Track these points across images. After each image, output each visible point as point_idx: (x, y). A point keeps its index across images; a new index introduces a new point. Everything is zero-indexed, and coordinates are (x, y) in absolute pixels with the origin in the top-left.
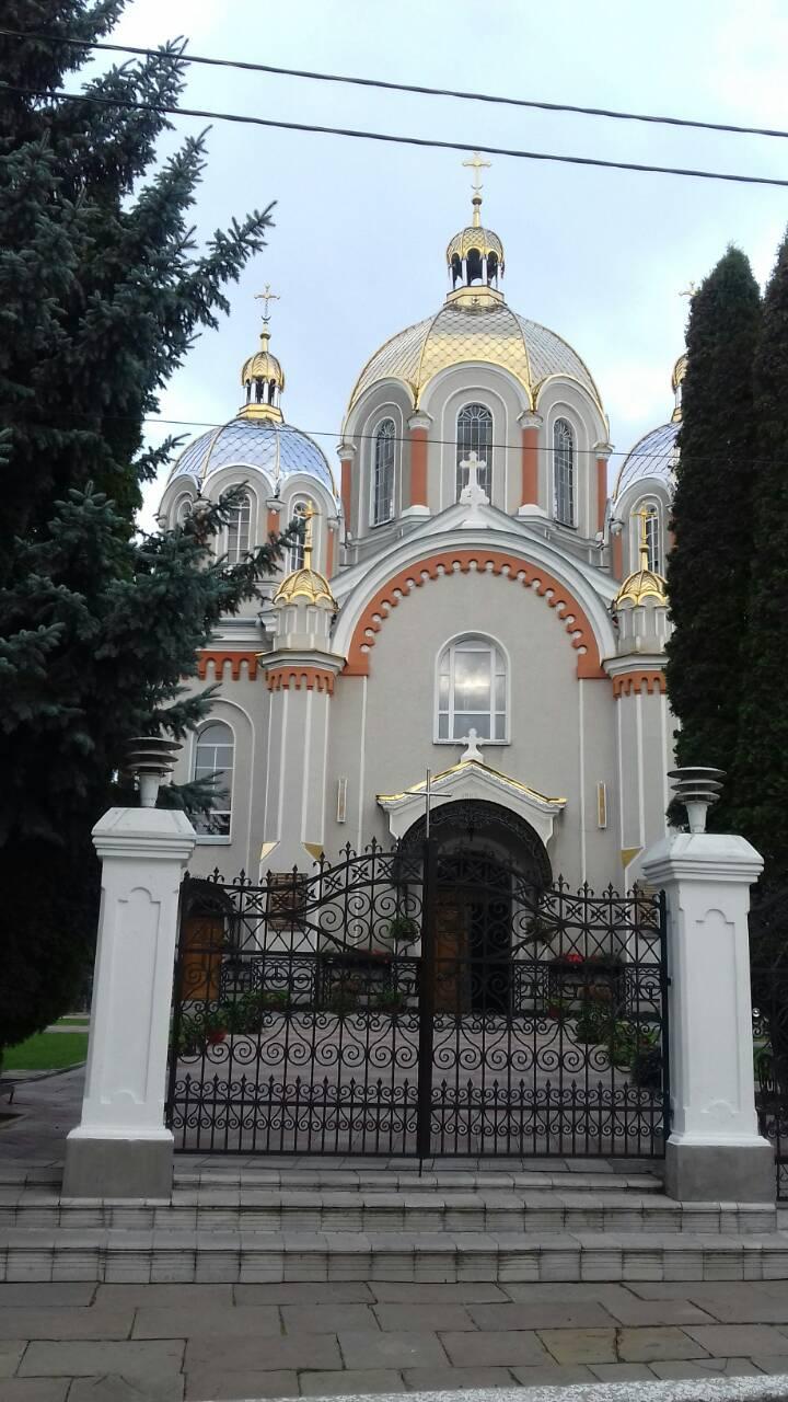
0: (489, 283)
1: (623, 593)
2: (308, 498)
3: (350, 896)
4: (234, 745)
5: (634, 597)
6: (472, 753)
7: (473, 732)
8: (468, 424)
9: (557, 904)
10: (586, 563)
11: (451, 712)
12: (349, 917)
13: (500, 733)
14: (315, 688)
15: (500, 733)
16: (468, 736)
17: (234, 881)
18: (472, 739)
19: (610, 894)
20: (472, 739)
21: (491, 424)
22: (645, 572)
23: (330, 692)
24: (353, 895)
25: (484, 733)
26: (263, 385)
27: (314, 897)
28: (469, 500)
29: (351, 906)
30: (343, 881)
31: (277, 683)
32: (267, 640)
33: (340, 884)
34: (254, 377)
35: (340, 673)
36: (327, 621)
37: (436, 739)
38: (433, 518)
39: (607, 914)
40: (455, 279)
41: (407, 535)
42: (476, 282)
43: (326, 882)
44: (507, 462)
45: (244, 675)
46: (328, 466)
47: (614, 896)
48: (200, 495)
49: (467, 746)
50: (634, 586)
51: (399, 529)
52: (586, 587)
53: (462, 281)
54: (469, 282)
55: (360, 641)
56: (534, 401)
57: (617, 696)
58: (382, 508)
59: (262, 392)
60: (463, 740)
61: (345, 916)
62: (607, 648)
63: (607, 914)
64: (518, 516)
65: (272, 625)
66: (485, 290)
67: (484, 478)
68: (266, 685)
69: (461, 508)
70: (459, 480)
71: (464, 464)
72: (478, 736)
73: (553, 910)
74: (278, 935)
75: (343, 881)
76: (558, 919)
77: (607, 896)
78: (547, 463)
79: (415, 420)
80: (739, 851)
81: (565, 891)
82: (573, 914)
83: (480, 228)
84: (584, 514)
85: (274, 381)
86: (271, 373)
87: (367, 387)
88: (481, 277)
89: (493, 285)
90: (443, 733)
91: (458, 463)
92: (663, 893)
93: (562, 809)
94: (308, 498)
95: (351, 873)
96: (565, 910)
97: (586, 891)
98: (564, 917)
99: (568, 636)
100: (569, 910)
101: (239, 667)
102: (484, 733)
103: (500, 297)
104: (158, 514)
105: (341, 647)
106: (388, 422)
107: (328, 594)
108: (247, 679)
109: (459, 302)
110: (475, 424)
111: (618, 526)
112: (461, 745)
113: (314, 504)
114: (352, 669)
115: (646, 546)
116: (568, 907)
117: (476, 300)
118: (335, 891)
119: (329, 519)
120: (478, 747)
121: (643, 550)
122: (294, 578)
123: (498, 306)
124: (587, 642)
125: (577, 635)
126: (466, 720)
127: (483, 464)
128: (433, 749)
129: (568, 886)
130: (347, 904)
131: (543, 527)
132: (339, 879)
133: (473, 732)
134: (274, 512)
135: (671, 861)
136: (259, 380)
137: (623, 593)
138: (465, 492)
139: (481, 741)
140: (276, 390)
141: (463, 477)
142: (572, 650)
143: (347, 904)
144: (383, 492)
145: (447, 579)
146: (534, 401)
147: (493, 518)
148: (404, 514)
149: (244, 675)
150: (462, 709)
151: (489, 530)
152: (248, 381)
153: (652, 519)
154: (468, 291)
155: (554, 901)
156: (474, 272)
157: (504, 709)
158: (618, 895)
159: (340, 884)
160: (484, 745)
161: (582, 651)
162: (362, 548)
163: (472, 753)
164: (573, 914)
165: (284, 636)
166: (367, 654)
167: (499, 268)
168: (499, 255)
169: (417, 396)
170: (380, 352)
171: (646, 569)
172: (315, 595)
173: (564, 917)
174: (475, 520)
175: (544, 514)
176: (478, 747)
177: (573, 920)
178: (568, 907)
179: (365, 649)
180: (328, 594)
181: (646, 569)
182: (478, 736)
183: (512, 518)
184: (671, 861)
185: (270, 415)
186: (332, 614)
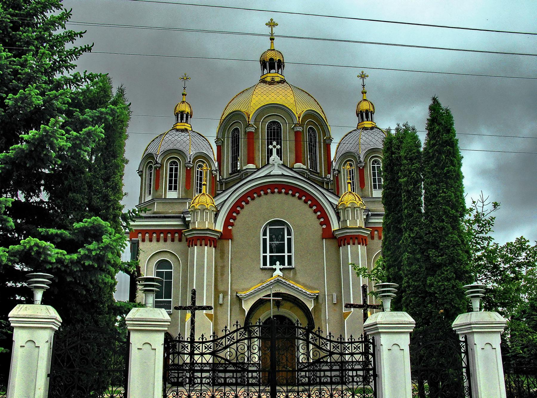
0: (278, 71)
1: (341, 202)
2: (204, 163)
3: (238, 344)
4: (173, 270)
5: (346, 204)
6: (278, 272)
7: (278, 263)
8: (271, 129)
9: (318, 340)
10: (323, 188)
11: (286, 254)
12: (238, 354)
13: (290, 263)
14: (208, 245)
15: (290, 263)
16: (276, 265)
17: (199, 339)
18: (278, 266)
19: (351, 339)
20: (278, 266)
21: (281, 129)
22: (350, 192)
23: (215, 247)
24: (240, 344)
25: (282, 263)
26: (183, 115)
27: (222, 345)
28: (274, 162)
29: (239, 348)
30: (235, 338)
31: (192, 242)
32: (186, 224)
33: (234, 339)
34: (179, 111)
35: (219, 239)
36: (213, 216)
37: (262, 266)
38: (258, 169)
39: (350, 348)
40: (264, 70)
41: (245, 178)
42: (272, 71)
43: (228, 338)
44: (288, 144)
45: (154, 239)
46: (211, 148)
47: (353, 340)
48: (157, 162)
49: (275, 269)
50: (346, 198)
51: (242, 174)
52: (325, 199)
53: (265, 71)
54: (270, 71)
55: (227, 223)
56: (299, 120)
57: (340, 246)
58: (234, 165)
59: (183, 118)
60: (274, 267)
61: (236, 353)
62: (335, 226)
63: (350, 348)
64: (293, 168)
65: (189, 217)
66: (276, 74)
67: (279, 152)
68: (186, 243)
69: (270, 165)
70: (268, 153)
71: (270, 147)
72: (280, 265)
73: (338, 350)
74: (208, 362)
75: (235, 338)
76: (330, 351)
77: (350, 341)
78: (306, 146)
79: (248, 128)
80: (405, 317)
81: (332, 339)
82: (336, 349)
83: (274, 50)
84: (321, 168)
85: (188, 113)
86: (188, 110)
87: (227, 114)
88: (275, 69)
89: (280, 72)
90: (265, 264)
91: (268, 146)
92: (373, 338)
93: (317, 296)
94: (204, 163)
95: (239, 334)
96: (332, 347)
97: (341, 339)
98: (332, 350)
99: (235, 224)
100: (334, 347)
101: (152, 235)
102: (282, 263)
103: (283, 77)
104: (138, 170)
105: (219, 227)
106: (237, 129)
107: (213, 204)
108: (163, 241)
109: (266, 79)
110: (274, 129)
111: (336, 172)
112: (273, 269)
113: (206, 166)
114: (226, 235)
115: (350, 181)
116: (333, 346)
117: (273, 79)
118: (232, 342)
119: (212, 171)
120: (280, 269)
121: (349, 183)
122: (198, 197)
123: (282, 81)
124: (327, 222)
125: (322, 220)
126: (275, 258)
127: (279, 147)
128: (261, 271)
129: (333, 337)
130: (237, 348)
131: (302, 172)
132: (233, 337)
133: (278, 263)
134: (189, 168)
135: (377, 324)
136: (182, 113)
137: (341, 202)
138: (271, 159)
139: (282, 267)
140: (189, 117)
141: (270, 152)
142: (320, 226)
143: (237, 348)
144: (235, 159)
145: (265, 196)
146: (299, 120)
147: (285, 170)
148: (244, 168)
149: (154, 239)
150: (273, 253)
151: (283, 175)
152: (177, 113)
153: (351, 169)
154: (269, 75)
155: (327, 343)
156: (272, 67)
157: (291, 253)
158: (354, 340)
159: (234, 339)
160: (283, 269)
161: (324, 227)
162: (226, 183)
163: (278, 272)
164: (336, 349)
165: (194, 223)
166: (231, 230)
167: (282, 66)
168: (281, 59)
169: (249, 118)
170: (233, 100)
171: (350, 191)
172: (208, 205)
173: (332, 350)
174: (277, 171)
175: (305, 167)
176: (280, 269)
177: (336, 351)
178: (333, 346)
179: (230, 228)
180: (213, 204)
181: (350, 191)
182: (280, 265)
183: (291, 169)
184: (377, 324)
185: (186, 127)
186: (215, 213)
